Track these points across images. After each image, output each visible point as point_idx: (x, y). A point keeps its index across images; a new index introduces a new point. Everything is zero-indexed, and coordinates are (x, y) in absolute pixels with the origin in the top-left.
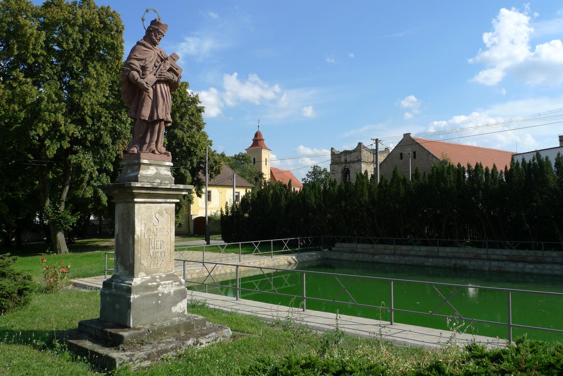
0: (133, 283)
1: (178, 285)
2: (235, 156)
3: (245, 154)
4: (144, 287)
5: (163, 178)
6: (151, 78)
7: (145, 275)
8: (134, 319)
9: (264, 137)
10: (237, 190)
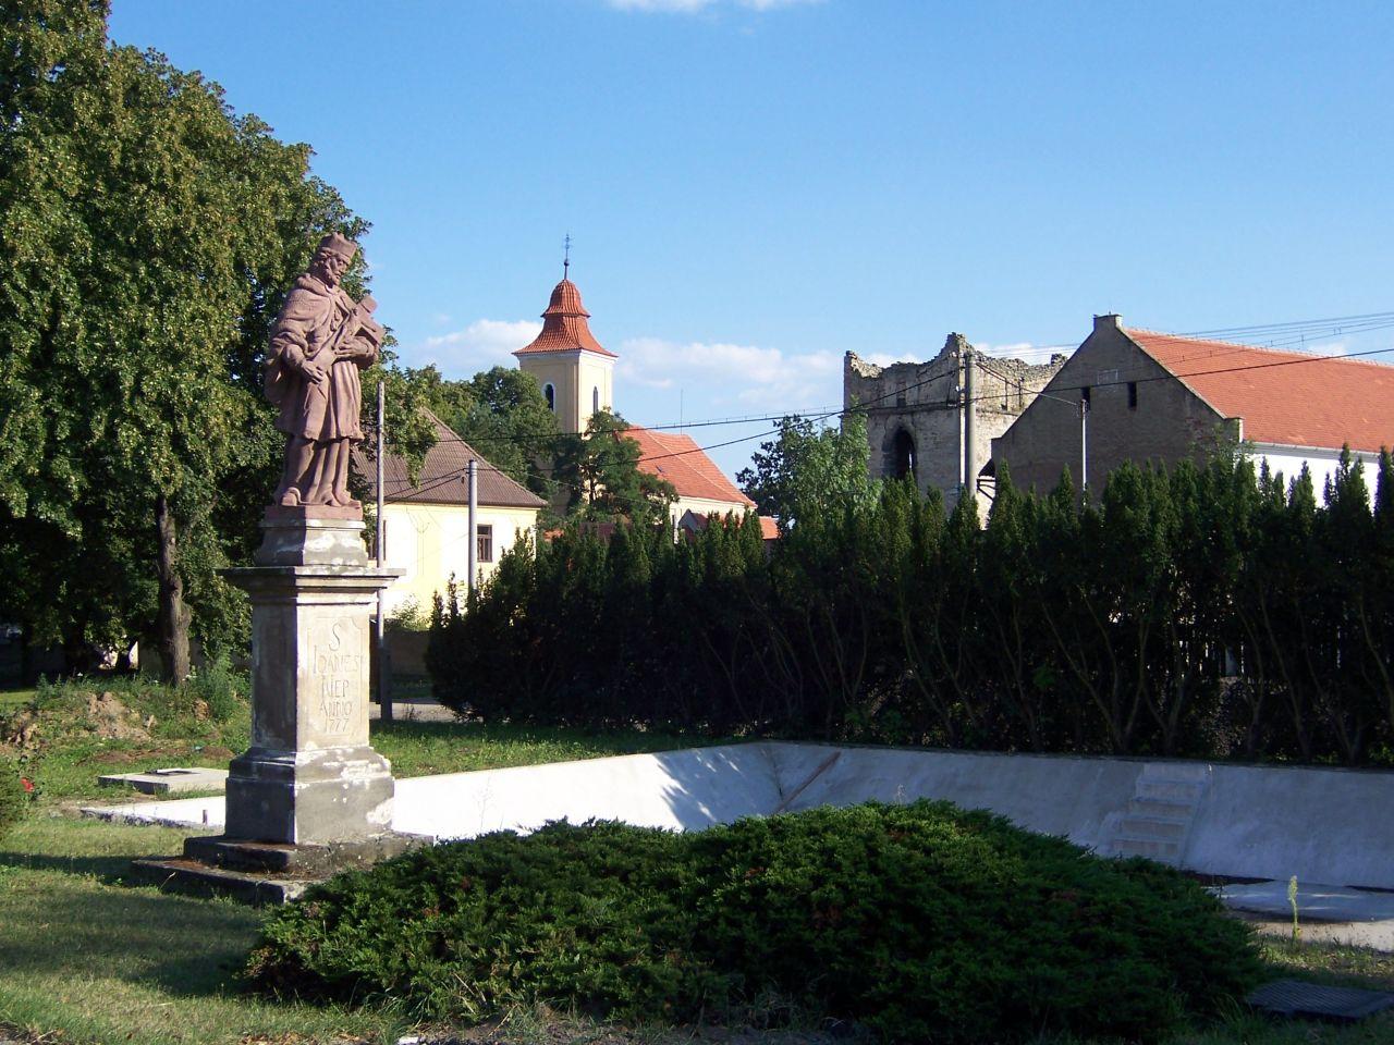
0: (297, 763)
1: (377, 770)
2: (477, 378)
3: (514, 371)
4: (317, 768)
5: (348, 554)
6: (326, 356)
7: (316, 748)
8: (302, 828)
9: (586, 305)
10: (483, 516)
